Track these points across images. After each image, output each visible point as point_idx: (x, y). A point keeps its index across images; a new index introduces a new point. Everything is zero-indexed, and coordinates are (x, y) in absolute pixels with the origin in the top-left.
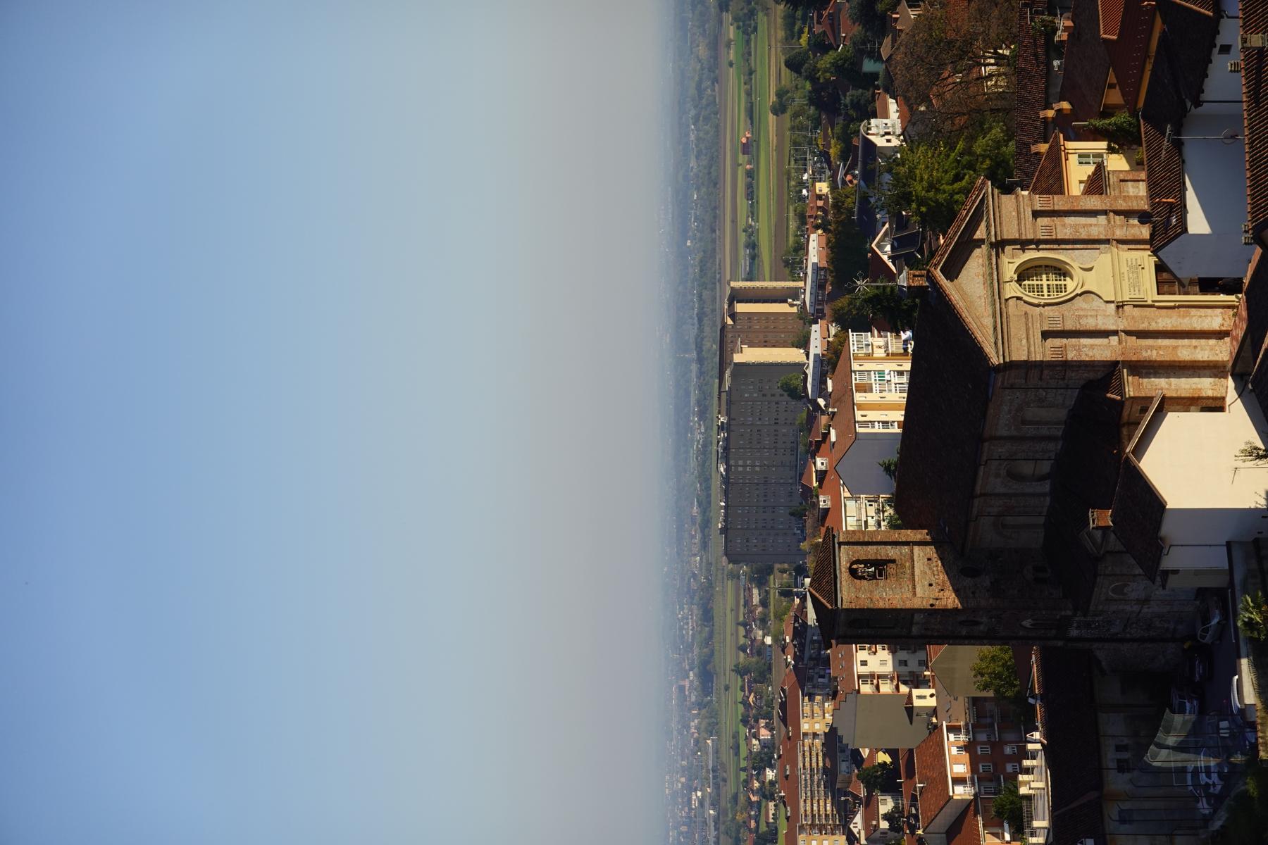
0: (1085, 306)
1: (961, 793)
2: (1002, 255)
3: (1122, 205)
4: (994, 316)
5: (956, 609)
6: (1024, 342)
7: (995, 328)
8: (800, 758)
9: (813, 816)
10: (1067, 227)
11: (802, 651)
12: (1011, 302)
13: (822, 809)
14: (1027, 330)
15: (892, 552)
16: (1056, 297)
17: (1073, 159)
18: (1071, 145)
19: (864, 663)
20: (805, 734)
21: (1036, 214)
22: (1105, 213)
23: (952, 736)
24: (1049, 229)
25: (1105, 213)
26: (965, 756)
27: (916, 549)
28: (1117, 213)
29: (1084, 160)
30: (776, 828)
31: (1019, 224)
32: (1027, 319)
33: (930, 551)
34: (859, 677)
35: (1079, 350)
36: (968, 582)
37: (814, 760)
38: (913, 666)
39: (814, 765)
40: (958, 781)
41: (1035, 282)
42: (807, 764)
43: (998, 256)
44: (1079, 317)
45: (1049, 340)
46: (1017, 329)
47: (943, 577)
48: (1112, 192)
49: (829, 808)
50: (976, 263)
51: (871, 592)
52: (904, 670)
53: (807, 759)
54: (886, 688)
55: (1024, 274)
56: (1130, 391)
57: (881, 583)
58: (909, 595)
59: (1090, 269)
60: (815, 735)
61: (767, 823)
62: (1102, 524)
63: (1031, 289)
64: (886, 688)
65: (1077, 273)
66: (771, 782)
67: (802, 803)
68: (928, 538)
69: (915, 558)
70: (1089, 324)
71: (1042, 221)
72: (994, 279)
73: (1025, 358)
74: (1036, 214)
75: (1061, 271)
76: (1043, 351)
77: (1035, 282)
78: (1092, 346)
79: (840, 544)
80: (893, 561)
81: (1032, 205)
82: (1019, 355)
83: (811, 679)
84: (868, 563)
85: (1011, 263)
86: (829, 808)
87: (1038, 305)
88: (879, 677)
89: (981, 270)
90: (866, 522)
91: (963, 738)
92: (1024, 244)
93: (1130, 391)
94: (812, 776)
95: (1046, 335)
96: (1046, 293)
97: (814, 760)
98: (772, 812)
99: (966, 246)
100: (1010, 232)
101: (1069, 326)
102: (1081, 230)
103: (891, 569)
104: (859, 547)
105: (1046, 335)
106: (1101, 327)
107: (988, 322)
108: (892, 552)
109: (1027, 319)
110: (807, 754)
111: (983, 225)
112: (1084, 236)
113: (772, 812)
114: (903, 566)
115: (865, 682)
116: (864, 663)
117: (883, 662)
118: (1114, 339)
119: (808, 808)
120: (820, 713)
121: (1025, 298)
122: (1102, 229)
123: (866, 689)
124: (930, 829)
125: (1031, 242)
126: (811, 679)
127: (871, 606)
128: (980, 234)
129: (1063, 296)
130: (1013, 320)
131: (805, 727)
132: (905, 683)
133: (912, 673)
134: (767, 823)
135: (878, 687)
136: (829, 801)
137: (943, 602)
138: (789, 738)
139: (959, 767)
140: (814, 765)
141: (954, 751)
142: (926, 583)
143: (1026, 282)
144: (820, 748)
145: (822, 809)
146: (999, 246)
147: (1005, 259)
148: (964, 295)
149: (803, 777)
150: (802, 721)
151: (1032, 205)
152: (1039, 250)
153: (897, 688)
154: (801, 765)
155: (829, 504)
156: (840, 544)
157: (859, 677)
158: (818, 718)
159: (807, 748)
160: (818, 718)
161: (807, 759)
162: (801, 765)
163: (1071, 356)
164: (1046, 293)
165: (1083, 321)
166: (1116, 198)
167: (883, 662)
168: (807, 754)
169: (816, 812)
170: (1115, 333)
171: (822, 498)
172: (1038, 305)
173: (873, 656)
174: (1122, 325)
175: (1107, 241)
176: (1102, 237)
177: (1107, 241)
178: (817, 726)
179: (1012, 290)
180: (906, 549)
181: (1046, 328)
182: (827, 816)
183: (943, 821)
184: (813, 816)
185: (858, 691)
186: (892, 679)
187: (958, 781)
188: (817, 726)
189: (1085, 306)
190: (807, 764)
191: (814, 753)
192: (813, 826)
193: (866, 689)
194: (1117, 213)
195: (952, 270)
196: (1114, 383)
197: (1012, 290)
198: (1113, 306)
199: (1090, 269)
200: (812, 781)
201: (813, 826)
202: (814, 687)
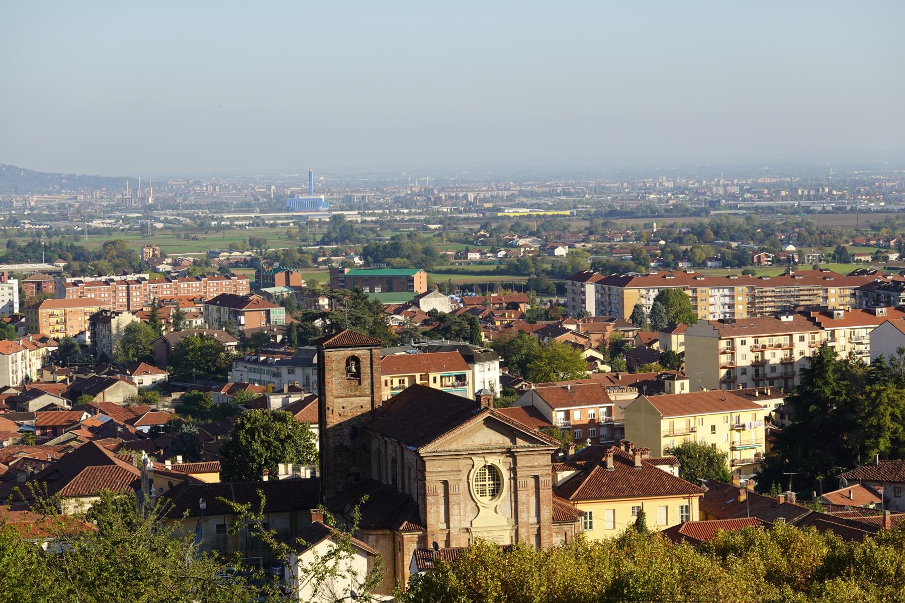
0: (469, 508)
1: (558, 417)
2: (503, 456)
3: (544, 533)
4: (456, 451)
5: (326, 424)
6: (440, 469)
7: (445, 451)
8: (771, 289)
9: (762, 298)
10: (527, 498)
11: (884, 288)
12: (470, 461)
13: (767, 304)
14: (448, 472)
15: (366, 383)
16: (474, 490)
17: (685, 502)
18: (695, 502)
19: (743, 343)
20: (826, 291)
21: (536, 478)
22: (539, 522)
23: (605, 410)
24: (525, 486)
25: (539, 522)
26: (586, 421)
27: (369, 398)
28: (539, 530)
29: (684, 509)
30: (849, 262)
31: (528, 467)
32: (456, 471)
33: (368, 408)
34: (732, 339)
35: (434, 504)
36: (347, 431)
37: (806, 298)
38: (741, 379)
39: (802, 298)
40: (568, 415)
41: (487, 477)
42: (802, 293)
43: (503, 453)
44: (459, 504)
45: (442, 485)
46: (448, 465)
47: (349, 416)
48: (555, 527)
49: (768, 309)
50: (502, 440)
51: (337, 370)
52: (738, 373)
53: (806, 293)
54: (724, 359)
55: (493, 469)
56: (407, 536)
57: (344, 376)
58: (335, 393)
59: (496, 512)
60: (826, 298)
61: (854, 255)
62: (313, 516)
63: (482, 474)
64: (724, 359)
65: (495, 503)
66: (887, 257)
67: (771, 289)
68: (376, 406)
69: (362, 398)
70: (454, 511)
71: (532, 482)
72: (485, 452)
73: (427, 469)
74: (536, 478)
75: (496, 492)
76: (433, 481)
77: (487, 477)
78: (438, 512)
79: (371, 350)
80: (360, 384)
81: (542, 476)
82: (429, 466)
83: (865, 295)
84: (358, 368)
85: (501, 463)
86: (768, 309)
87: (468, 478)
88: (733, 354)
89: (494, 442)
90: (861, 343)
91: (602, 418)
92: (513, 470)
93: (407, 536)
94: (793, 296)
95: (445, 483)
96: (479, 483)
97: (806, 298)
98: (863, 258)
99: (511, 433)
100: (521, 461)
101: (452, 498)
102: (524, 506)
103: (354, 382)
104: (369, 362)
105: (445, 483)
106: (451, 519)
107: (454, 446)
108: (366, 383)
109: (456, 471)
110: (811, 292)
111: (526, 444)
112: (520, 508)
113: (863, 258)
114: (356, 390)
115: (729, 343)
116: (743, 343)
117: (744, 357)
118: (444, 526)
119: (767, 294)
120: (844, 302)
121: (473, 470)
122: (525, 519)
123: (723, 345)
124: (535, 395)
125: (515, 474)
126: (865, 295)
127: (327, 370)
128: (520, 442)
129: (477, 497)
130: (456, 462)
131: (832, 291)
132: (728, 373)
133: (735, 378)
134: (854, 255)
135: (724, 353)
136: (774, 309)
137: (330, 416)
138: (824, 278)
139: (578, 415)
140: (802, 298)
141: (591, 412)
142: (344, 405)
143: (487, 471)
144: (815, 303)
145: (767, 304)
146: (510, 453)
147: (502, 457)
148: (474, 431)
149: (793, 290)
150: (837, 289)
151: (542, 476)
152: (510, 479)
153: (724, 367)
154: (765, 289)
155: (879, 315)
156: (371, 350)
157: (732, 339)
158: (839, 300)
159: (815, 292)
160: (839, 300)
161: (806, 293)
162: (765, 289)
163: (430, 499)
164: (479, 483)
165: (456, 507)
166: (549, 529)
167: (744, 357)
168: (811, 292)
169: (765, 299)
170: (448, 527)
171: (884, 310)
172: (468, 478)
173: (749, 349)
174: (454, 531)
175: (517, 523)
176: (520, 520)
177: (517, 523)
178: (833, 300)
179: (479, 462)
180: (368, 392)
181: (450, 483)
182: (762, 308)
183: (539, 404)
184: (762, 298)
185: (720, 339)
186: (731, 363)
187: (568, 415)
188: (833, 300)
189: (469, 508)
190: (802, 293)
191: (811, 298)
192: (754, 297)
193: (723, 345)
194: (539, 530)
195: (490, 423)
196: (412, 526)
197: (479, 462)
198: (468, 526)
199: (496, 512)
200: (789, 297)
201: (754, 297)
202: (860, 297)
